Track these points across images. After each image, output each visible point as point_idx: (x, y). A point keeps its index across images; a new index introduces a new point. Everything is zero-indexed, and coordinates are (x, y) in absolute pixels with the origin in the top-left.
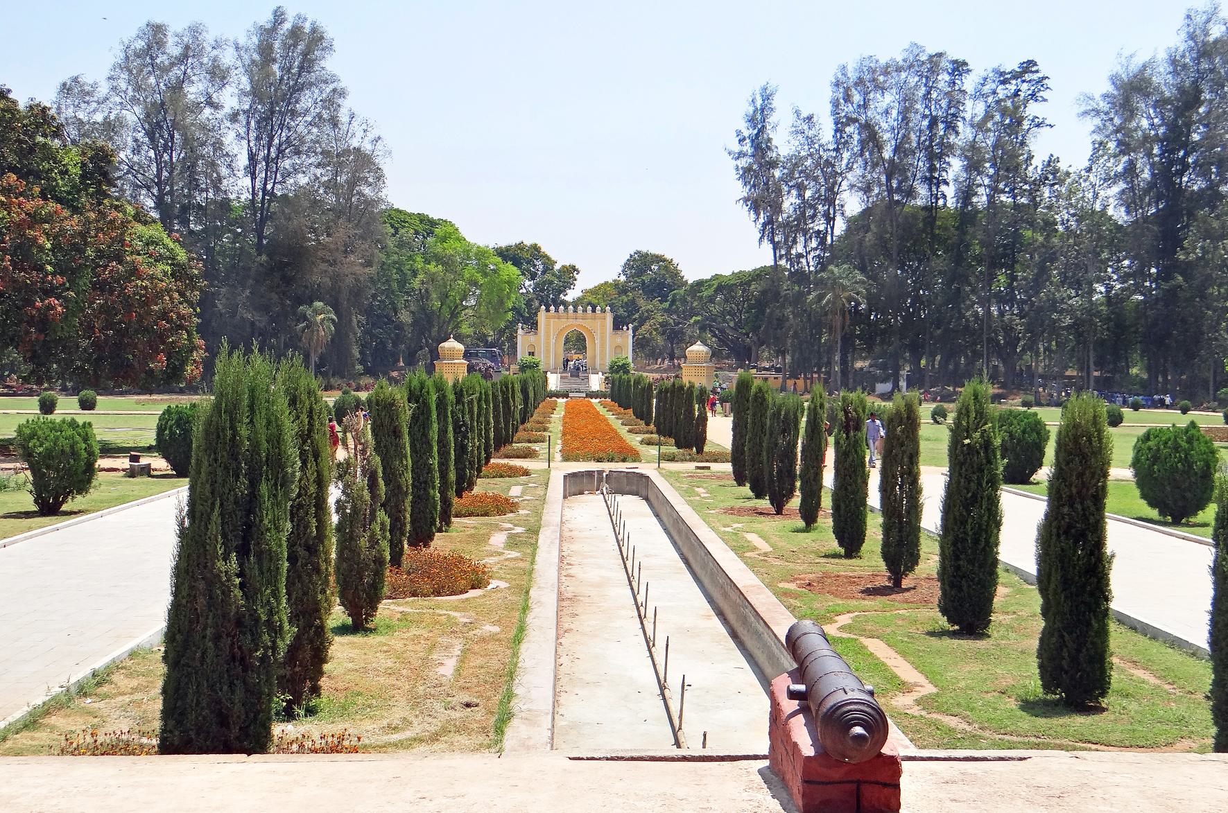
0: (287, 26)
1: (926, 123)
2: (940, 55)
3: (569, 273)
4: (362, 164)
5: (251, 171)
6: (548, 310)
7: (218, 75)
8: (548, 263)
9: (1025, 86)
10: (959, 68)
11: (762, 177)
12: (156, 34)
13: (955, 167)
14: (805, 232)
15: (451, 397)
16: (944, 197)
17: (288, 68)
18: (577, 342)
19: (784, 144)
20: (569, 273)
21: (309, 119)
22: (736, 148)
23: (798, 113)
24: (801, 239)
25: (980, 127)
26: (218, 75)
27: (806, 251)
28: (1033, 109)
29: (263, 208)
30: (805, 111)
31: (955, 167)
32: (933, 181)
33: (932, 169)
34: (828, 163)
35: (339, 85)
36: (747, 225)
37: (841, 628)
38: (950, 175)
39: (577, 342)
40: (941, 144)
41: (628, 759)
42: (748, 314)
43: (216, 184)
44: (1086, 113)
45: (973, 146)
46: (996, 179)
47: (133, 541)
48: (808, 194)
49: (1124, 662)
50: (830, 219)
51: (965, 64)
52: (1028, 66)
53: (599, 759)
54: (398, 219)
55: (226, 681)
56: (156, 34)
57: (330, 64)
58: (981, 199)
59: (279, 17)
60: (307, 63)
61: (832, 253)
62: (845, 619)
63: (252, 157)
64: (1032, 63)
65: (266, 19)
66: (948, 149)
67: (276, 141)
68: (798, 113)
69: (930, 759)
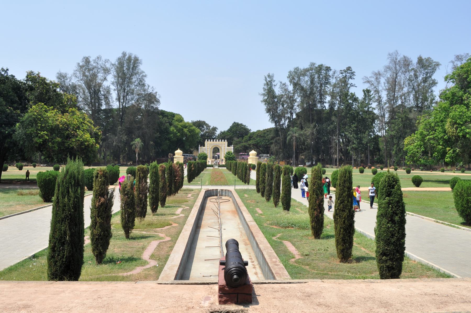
0: (127, 56)
1: (319, 85)
2: (322, 65)
3: (215, 129)
4: (151, 98)
5: (119, 99)
6: (208, 141)
7: (107, 71)
8: (208, 126)
9: (348, 74)
10: (328, 69)
11: (272, 102)
12: (87, 61)
13: (328, 98)
14: (284, 117)
15: (160, 173)
16: (325, 107)
17: (127, 69)
18: (216, 150)
19: (278, 91)
20: (215, 129)
21: (136, 84)
22: (263, 92)
23: (281, 83)
24: (283, 120)
25: (335, 86)
26: (107, 71)
27: (285, 123)
28: (350, 81)
29: (123, 110)
30: (282, 83)
31: (328, 98)
32: (322, 102)
33: (321, 98)
34: (291, 97)
35: (144, 74)
36: (267, 117)
37: (279, 238)
38: (327, 101)
39: (216, 150)
40: (324, 91)
41: (177, 284)
42: (262, 142)
43: (108, 103)
44: (365, 82)
45: (333, 92)
46: (340, 102)
47: (35, 226)
48: (285, 106)
49: (358, 249)
50: (292, 114)
51: (330, 68)
52: (349, 68)
53: (167, 284)
54: (163, 113)
55: (64, 262)
56: (87, 61)
57: (142, 67)
58: (336, 108)
59: (124, 54)
60: (135, 67)
61: (292, 123)
62: (279, 235)
63: (119, 95)
64: (350, 67)
65: (120, 55)
66: (326, 93)
67: (126, 91)
68: (281, 83)
69: (269, 283)
